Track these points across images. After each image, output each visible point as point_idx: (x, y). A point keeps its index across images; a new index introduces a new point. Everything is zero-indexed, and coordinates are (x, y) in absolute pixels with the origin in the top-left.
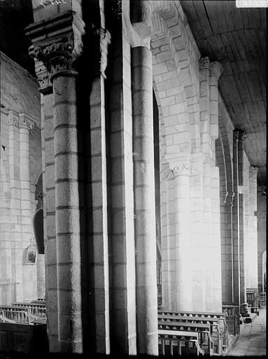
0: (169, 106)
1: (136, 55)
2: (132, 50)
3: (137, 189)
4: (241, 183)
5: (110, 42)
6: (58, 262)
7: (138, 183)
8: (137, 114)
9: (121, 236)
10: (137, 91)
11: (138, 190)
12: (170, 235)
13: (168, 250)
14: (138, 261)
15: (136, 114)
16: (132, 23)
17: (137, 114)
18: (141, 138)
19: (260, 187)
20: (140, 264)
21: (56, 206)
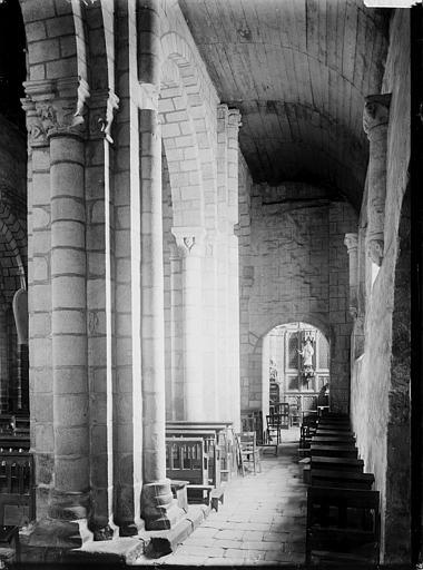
0: (185, 147)
1: (143, 117)
2: (140, 111)
3: (145, 319)
4: (146, 73)
5: (88, 94)
6: (55, 365)
7: (146, 312)
8: (145, 179)
9: (126, 261)
10: (145, 154)
11: (146, 320)
12: (176, 273)
13: (173, 292)
14: (145, 389)
15: (144, 210)
16: (139, 78)
17: (145, 179)
18: (150, 180)
19: (258, 186)
20: (147, 370)
21: (54, 306)
